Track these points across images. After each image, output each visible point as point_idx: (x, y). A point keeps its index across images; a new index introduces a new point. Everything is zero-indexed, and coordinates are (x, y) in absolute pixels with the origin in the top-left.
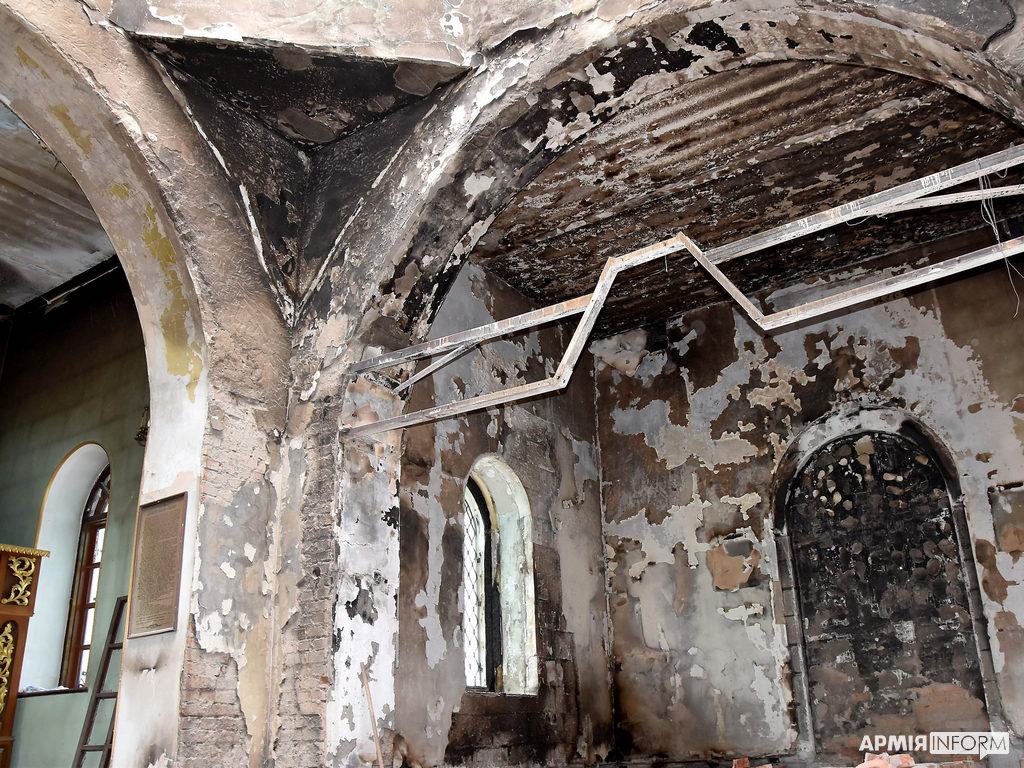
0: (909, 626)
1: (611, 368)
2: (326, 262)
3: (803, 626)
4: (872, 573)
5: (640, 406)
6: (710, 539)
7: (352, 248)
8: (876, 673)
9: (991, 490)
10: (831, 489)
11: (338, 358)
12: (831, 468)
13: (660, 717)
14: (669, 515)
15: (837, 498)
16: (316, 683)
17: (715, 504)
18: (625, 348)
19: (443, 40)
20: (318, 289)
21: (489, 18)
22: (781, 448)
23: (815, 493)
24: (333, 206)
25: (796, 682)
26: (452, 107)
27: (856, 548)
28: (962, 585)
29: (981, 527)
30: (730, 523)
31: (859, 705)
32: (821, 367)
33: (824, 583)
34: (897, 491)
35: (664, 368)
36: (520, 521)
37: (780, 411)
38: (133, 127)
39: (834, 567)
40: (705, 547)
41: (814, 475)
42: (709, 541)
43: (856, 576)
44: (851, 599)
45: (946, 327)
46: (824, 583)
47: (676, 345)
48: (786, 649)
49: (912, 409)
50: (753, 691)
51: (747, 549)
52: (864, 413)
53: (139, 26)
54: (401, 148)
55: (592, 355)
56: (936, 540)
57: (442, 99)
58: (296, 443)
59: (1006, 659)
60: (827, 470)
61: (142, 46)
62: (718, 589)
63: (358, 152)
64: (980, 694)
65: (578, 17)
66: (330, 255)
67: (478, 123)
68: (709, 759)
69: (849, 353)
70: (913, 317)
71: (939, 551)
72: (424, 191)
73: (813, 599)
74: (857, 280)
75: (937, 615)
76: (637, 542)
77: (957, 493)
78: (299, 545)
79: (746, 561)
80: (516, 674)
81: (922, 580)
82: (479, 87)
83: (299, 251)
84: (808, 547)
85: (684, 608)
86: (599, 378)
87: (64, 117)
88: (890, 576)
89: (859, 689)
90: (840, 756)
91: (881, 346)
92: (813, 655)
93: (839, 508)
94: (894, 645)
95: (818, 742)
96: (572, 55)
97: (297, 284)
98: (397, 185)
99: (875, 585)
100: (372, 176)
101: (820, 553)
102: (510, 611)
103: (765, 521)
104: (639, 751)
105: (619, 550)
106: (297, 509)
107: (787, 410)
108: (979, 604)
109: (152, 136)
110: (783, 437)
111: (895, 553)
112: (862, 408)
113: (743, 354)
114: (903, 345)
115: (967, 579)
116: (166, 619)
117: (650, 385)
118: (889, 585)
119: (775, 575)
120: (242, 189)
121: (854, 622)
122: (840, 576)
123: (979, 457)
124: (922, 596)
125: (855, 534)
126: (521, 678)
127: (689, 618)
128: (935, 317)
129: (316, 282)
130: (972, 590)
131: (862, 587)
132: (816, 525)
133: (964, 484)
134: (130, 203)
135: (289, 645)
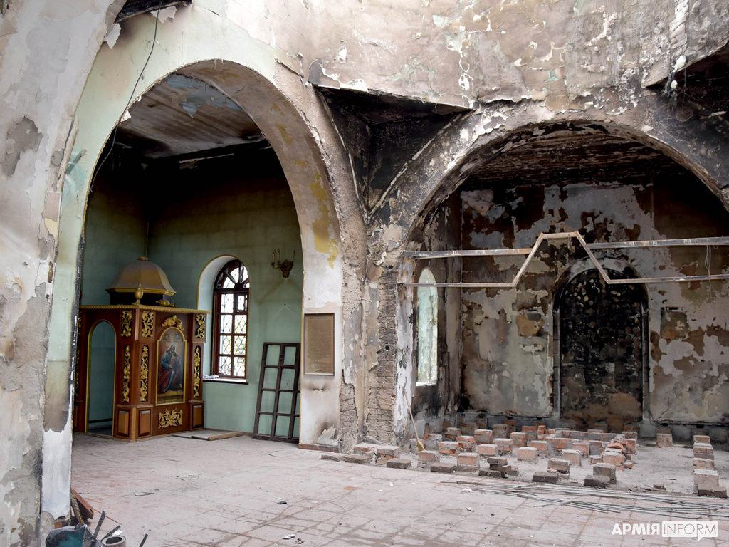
0: (613, 365)
1: (471, 208)
2: (386, 193)
3: (561, 358)
4: (597, 337)
5: (487, 233)
6: (520, 309)
7: (402, 190)
8: (594, 385)
9: (663, 309)
10: (584, 294)
11: (397, 248)
12: (585, 283)
13: (485, 393)
14: (498, 294)
15: (586, 299)
16: (389, 397)
17: (524, 293)
18: (481, 199)
19: (459, 94)
20: (382, 207)
21: (484, 84)
22: (562, 269)
23: (575, 294)
24: (387, 162)
25: (555, 385)
26: (460, 128)
27: (592, 325)
28: (641, 350)
29: (654, 325)
30: (530, 303)
31: (584, 398)
32: (588, 231)
33: (574, 339)
34: (617, 300)
35: (502, 215)
36: (431, 297)
37: (563, 250)
38: (317, 138)
39: (580, 332)
40: (516, 313)
41: (576, 285)
42: (519, 311)
43: (590, 338)
44: (586, 349)
45: (655, 224)
46: (574, 339)
47: (510, 203)
48: (552, 369)
49: (631, 262)
50: (533, 386)
51: (538, 317)
52: (607, 259)
53: (320, 82)
54: (430, 142)
55: (462, 199)
56: (632, 327)
57: (454, 120)
58: (373, 285)
59: (655, 387)
60: (583, 284)
61: (318, 90)
62: (521, 335)
63: (402, 135)
64: (640, 400)
65: (535, 102)
66: (388, 190)
67: (476, 143)
68: (508, 415)
69: (604, 226)
70: (640, 214)
71: (632, 332)
72: (446, 172)
73: (567, 346)
74: (614, 188)
75: (626, 362)
76: (480, 306)
77: (646, 307)
78: (377, 335)
79: (537, 324)
80: (425, 373)
81: (622, 345)
82: (477, 122)
83: (368, 182)
84: (569, 320)
85: (503, 342)
86: (465, 213)
87: (283, 129)
88: (607, 340)
89: (584, 391)
90: (571, 420)
91: (621, 226)
92: (564, 372)
93: (587, 304)
94: (604, 373)
95: (562, 412)
96: (530, 123)
97: (368, 201)
98: (428, 163)
99: (599, 344)
100: (412, 152)
101: (574, 324)
102: (423, 342)
103: (549, 305)
104: (472, 408)
105: (470, 308)
106: (375, 318)
107: (567, 251)
108: (648, 360)
109: (323, 140)
110: (564, 264)
111: (611, 330)
112: (606, 257)
113: (547, 215)
114: (632, 228)
115: (644, 348)
116: (329, 369)
117: (493, 223)
118: (606, 345)
119: (551, 333)
120: (350, 155)
121: (586, 360)
122: (582, 337)
123: (660, 292)
124: (621, 352)
125: (593, 318)
126: (428, 375)
127: (504, 347)
128: (651, 217)
129: (380, 203)
130: (645, 354)
131: (592, 343)
132: (574, 310)
133: (651, 304)
134: (306, 170)
135: (373, 379)
